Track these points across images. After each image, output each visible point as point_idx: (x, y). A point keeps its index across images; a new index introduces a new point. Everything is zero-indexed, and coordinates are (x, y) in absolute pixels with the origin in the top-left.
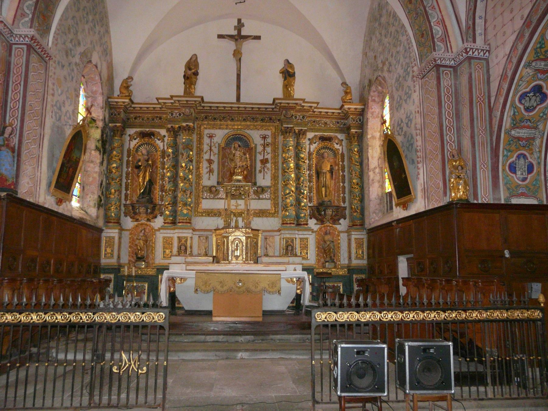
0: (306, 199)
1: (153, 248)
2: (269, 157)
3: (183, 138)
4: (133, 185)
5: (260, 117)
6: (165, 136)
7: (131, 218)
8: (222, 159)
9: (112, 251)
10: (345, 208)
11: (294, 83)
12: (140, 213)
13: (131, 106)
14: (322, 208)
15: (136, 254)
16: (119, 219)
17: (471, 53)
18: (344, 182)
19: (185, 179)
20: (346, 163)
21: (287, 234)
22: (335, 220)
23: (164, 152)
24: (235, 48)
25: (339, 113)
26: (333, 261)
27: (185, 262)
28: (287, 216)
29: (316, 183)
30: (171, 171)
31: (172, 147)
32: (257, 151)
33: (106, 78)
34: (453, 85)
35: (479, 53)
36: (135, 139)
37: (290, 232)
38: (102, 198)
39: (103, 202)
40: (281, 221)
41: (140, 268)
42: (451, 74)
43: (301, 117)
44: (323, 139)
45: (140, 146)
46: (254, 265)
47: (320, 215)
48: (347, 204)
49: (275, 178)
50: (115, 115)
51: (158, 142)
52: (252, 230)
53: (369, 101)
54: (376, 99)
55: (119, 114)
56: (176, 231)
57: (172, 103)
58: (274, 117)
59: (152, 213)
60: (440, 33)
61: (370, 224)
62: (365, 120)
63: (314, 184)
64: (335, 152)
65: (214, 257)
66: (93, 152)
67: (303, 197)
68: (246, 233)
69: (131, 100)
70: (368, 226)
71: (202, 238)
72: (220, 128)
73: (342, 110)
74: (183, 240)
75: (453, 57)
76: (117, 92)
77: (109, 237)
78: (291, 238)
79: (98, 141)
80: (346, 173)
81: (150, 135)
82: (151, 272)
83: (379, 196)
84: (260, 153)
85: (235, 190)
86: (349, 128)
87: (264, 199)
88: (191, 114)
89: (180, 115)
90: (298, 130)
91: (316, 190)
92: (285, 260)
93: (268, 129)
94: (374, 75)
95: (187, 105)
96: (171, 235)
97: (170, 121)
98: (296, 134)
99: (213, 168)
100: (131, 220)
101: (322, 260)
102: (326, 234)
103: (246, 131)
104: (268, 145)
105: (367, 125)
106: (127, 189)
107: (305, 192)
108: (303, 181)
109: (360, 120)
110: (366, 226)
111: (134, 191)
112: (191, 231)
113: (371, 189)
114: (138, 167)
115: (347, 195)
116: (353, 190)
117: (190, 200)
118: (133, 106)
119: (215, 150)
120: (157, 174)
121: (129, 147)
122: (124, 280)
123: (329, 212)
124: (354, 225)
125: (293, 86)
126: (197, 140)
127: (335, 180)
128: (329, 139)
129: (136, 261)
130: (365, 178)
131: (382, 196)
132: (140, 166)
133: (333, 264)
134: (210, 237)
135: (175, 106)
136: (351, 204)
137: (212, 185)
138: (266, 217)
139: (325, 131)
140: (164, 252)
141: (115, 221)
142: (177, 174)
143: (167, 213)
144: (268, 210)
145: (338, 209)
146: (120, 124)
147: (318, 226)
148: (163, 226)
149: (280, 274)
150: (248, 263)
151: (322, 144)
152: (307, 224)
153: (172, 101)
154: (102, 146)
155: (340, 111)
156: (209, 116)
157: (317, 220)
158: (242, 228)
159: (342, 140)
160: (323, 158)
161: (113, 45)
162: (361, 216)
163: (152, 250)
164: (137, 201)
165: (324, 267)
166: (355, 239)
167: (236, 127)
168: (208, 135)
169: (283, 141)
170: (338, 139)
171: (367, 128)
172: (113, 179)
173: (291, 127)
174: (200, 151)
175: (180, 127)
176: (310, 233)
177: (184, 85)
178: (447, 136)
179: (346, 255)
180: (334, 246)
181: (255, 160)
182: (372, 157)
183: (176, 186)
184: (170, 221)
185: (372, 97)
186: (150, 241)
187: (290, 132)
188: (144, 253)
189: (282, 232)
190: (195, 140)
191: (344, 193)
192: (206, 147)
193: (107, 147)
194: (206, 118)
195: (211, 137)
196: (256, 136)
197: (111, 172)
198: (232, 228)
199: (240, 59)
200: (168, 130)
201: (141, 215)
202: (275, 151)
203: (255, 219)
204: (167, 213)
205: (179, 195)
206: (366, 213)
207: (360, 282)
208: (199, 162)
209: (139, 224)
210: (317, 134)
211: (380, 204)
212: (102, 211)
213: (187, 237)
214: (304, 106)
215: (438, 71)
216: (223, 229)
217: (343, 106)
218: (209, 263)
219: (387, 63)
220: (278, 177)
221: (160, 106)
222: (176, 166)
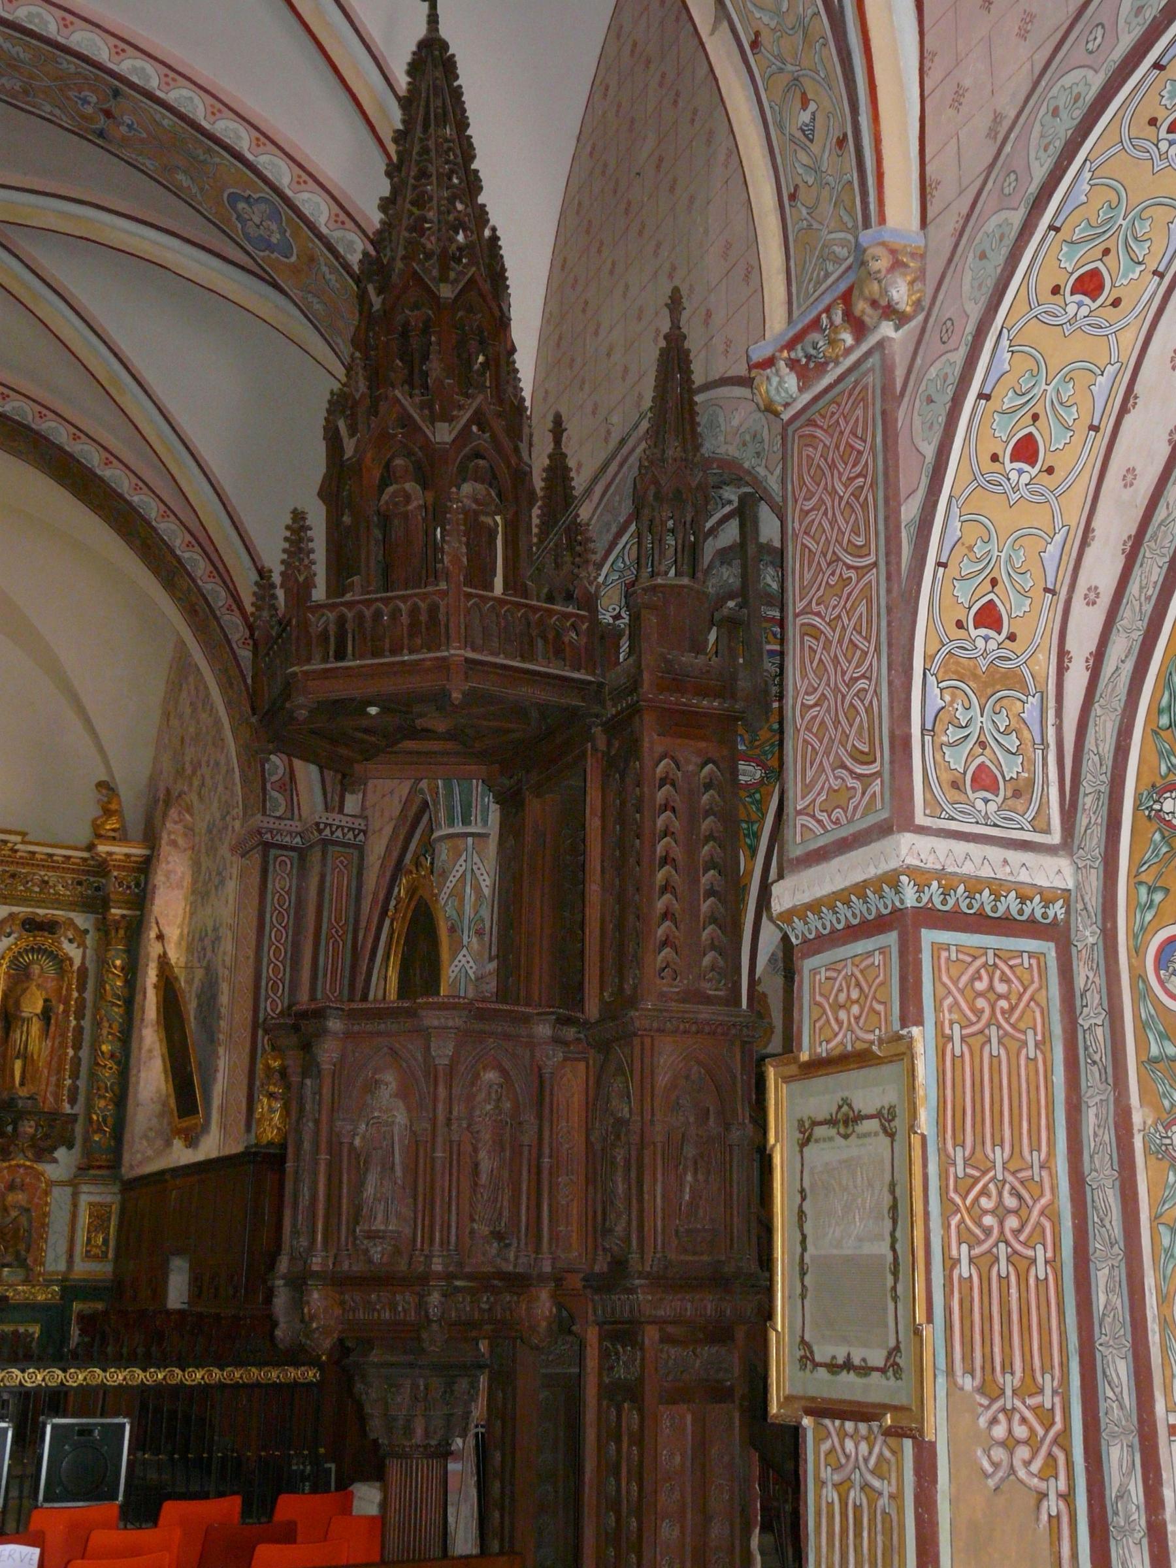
10: (73, 1118)
17: (327, 832)
22: (43, 1152)
25: (85, 860)
34: (294, 889)
35: (344, 835)
42: (292, 864)
44: (32, 925)
53: (163, 842)
60: (281, 771)
62: (150, 887)
64: (61, 962)
70: (127, 1172)
75: (299, 829)
80: (86, 1023)
109: (138, 885)
110: (123, 1170)
115: (82, 1084)
123: (28, 1128)
124: (90, 1167)
127: (54, 1038)
128: (50, 927)
136: (89, 1107)
139: (40, 903)
151: (29, 940)
155: (85, 855)
159: (86, 931)
166: (90, 1204)
170: (76, 928)
178: (266, 1000)
179: (63, 1247)
180: (30, 1222)
191: (75, 1075)
206: (127, 1136)
207: (88, 1322)
210: (15, 909)
211: (161, 1115)
215: (265, 857)
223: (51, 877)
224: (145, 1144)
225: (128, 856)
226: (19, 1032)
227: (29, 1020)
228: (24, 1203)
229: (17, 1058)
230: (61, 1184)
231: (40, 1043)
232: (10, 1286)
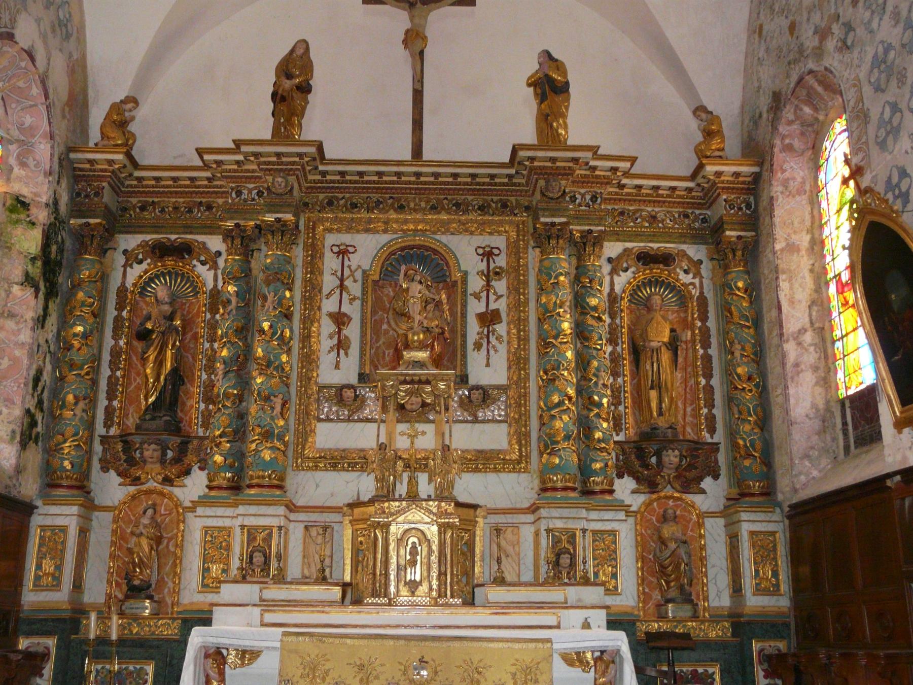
0: (607, 420)
1: (178, 560)
2: (501, 305)
3: (266, 256)
4: (130, 384)
5: (476, 201)
6: (219, 254)
7: (119, 475)
8: (374, 313)
9: (59, 567)
10: (715, 447)
11: (567, 108)
12: (145, 462)
13: (131, 175)
14: (652, 448)
15: (128, 578)
16: (85, 475)
18: (708, 376)
19: (269, 364)
20: (711, 323)
21: (557, 518)
22: (689, 482)
23: (215, 294)
24: (408, 25)
25: (690, 190)
26: (687, 599)
27: (262, 600)
28: (555, 469)
29: (633, 379)
30: (233, 344)
31: (235, 279)
32: (470, 291)
33: (65, 98)
36: (140, 262)
37: (565, 512)
38: (39, 417)
39: (39, 428)
40: (536, 484)
41: (136, 618)
43: (588, 197)
44: (646, 258)
45: (151, 280)
46: (465, 610)
47: (647, 466)
48: (719, 437)
49: (517, 362)
50: (87, 196)
51: (201, 270)
52: (458, 505)
53: (776, 150)
54: (797, 144)
55: (97, 194)
56: (241, 509)
57: (238, 162)
58: (513, 199)
59: (177, 460)
61: (796, 491)
62: (764, 203)
63: (626, 380)
65: (345, 586)
66: (16, 289)
67: (598, 415)
68: (442, 514)
69: (129, 155)
71: (314, 532)
72: (367, 231)
73: (700, 180)
74: (260, 537)
76: (95, 135)
77: (53, 528)
78: (567, 531)
79: (33, 260)
81: (184, 251)
82: (168, 629)
83: (817, 410)
84: (477, 296)
85: (409, 393)
86: (718, 229)
87: (489, 421)
88: (287, 191)
89: (260, 193)
90: (581, 232)
91: (634, 402)
92: (555, 594)
93: (500, 233)
94: (788, 76)
95: (279, 166)
96: (227, 523)
97: (232, 211)
98: (576, 244)
99: (346, 337)
100: (119, 480)
101: (657, 596)
102: (664, 519)
103: (437, 237)
104: (497, 274)
105: (772, 217)
106: (111, 396)
107: (605, 401)
108: (598, 369)
109: (748, 206)
110: (780, 497)
111: (131, 400)
112: (281, 510)
113: (792, 391)
114: (144, 335)
116: (737, 394)
117: (282, 423)
118: (137, 174)
119: (355, 288)
120: (194, 358)
121: (123, 284)
122: (85, 654)
123: (672, 457)
124: (743, 495)
125: (564, 116)
126: (305, 262)
128: (666, 259)
129: (127, 597)
130: (772, 362)
131: (828, 409)
132: (151, 332)
133: (688, 607)
134: (336, 527)
135: (248, 171)
136: (732, 434)
137: (345, 382)
138: (495, 470)
139: (653, 238)
140: (206, 570)
141: (74, 483)
142: (248, 350)
143: (218, 458)
144: (499, 452)
145: (697, 449)
146: (98, 221)
147: (641, 499)
148: (205, 496)
149: (549, 641)
150: (447, 605)
151: (645, 274)
152: (611, 492)
153: (240, 158)
154: (44, 274)
155: (691, 184)
156: (338, 199)
157: (638, 480)
158: (429, 498)
159: (700, 262)
160: (649, 309)
161: (88, 18)
162: (765, 469)
163: (175, 565)
164: (138, 427)
165: (662, 617)
166: (752, 533)
167: (412, 227)
168: (336, 249)
169: (541, 261)
170: (690, 259)
171: (772, 225)
172: (72, 366)
173: (560, 224)
174: (312, 291)
175: (257, 226)
176: (622, 515)
177: (272, 120)
180: (689, 555)
181: (464, 315)
182: (792, 302)
183: (244, 382)
184: (224, 484)
185: (783, 138)
186: (170, 539)
187: (558, 237)
188: (151, 574)
189: (543, 512)
190: (299, 261)
191: (711, 405)
192: (329, 282)
193: (60, 279)
194: (330, 203)
195: (343, 252)
196: (465, 250)
197: (69, 348)
198: (400, 499)
199: (421, 53)
200: (228, 236)
201: (149, 467)
202: (517, 289)
203: (466, 476)
204: (218, 458)
205: (253, 409)
206: (780, 459)
208: (308, 321)
209: (139, 492)
210: (629, 245)
211: (822, 431)
212: (34, 456)
213: (270, 528)
214: (594, 168)
216: (372, 501)
217: (701, 167)
218: (331, 603)
219: (835, 28)
220: (527, 360)
221: (208, 174)
222: (245, 330)
223: (660, 211)
224: (807, 463)
225: (737, 175)
226: (649, 362)
227: (658, 350)
228: (679, 535)
229: (652, 388)
230: (712, 514)
231: (672, 373)
232: (679, 622)
